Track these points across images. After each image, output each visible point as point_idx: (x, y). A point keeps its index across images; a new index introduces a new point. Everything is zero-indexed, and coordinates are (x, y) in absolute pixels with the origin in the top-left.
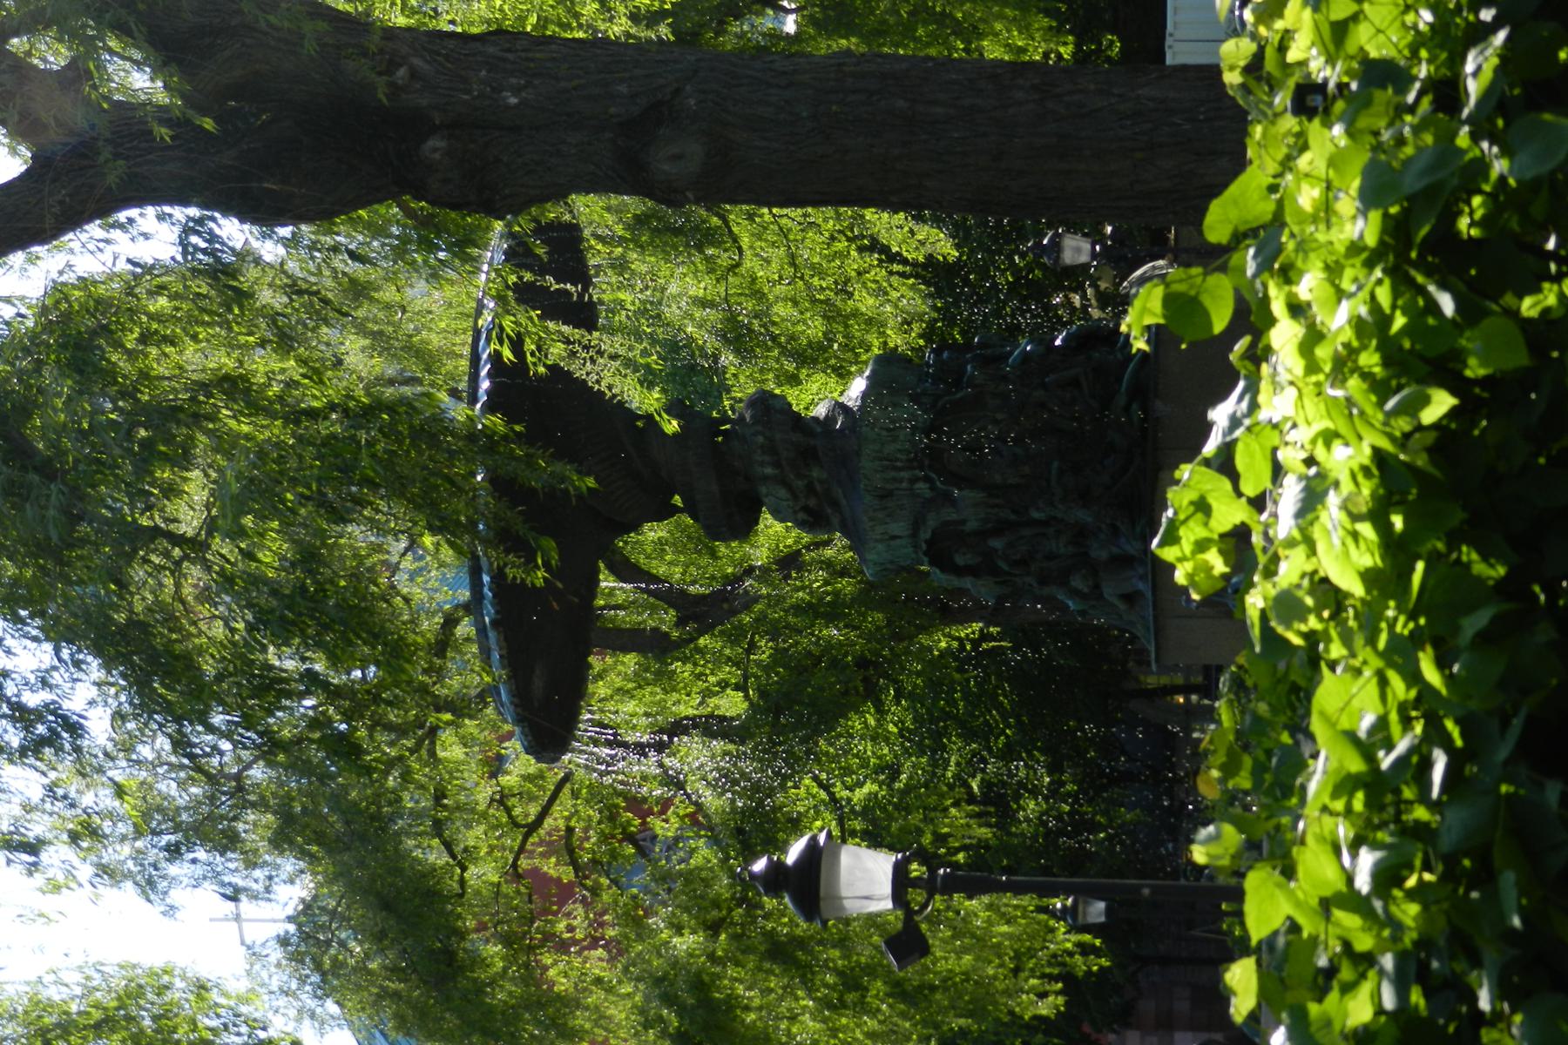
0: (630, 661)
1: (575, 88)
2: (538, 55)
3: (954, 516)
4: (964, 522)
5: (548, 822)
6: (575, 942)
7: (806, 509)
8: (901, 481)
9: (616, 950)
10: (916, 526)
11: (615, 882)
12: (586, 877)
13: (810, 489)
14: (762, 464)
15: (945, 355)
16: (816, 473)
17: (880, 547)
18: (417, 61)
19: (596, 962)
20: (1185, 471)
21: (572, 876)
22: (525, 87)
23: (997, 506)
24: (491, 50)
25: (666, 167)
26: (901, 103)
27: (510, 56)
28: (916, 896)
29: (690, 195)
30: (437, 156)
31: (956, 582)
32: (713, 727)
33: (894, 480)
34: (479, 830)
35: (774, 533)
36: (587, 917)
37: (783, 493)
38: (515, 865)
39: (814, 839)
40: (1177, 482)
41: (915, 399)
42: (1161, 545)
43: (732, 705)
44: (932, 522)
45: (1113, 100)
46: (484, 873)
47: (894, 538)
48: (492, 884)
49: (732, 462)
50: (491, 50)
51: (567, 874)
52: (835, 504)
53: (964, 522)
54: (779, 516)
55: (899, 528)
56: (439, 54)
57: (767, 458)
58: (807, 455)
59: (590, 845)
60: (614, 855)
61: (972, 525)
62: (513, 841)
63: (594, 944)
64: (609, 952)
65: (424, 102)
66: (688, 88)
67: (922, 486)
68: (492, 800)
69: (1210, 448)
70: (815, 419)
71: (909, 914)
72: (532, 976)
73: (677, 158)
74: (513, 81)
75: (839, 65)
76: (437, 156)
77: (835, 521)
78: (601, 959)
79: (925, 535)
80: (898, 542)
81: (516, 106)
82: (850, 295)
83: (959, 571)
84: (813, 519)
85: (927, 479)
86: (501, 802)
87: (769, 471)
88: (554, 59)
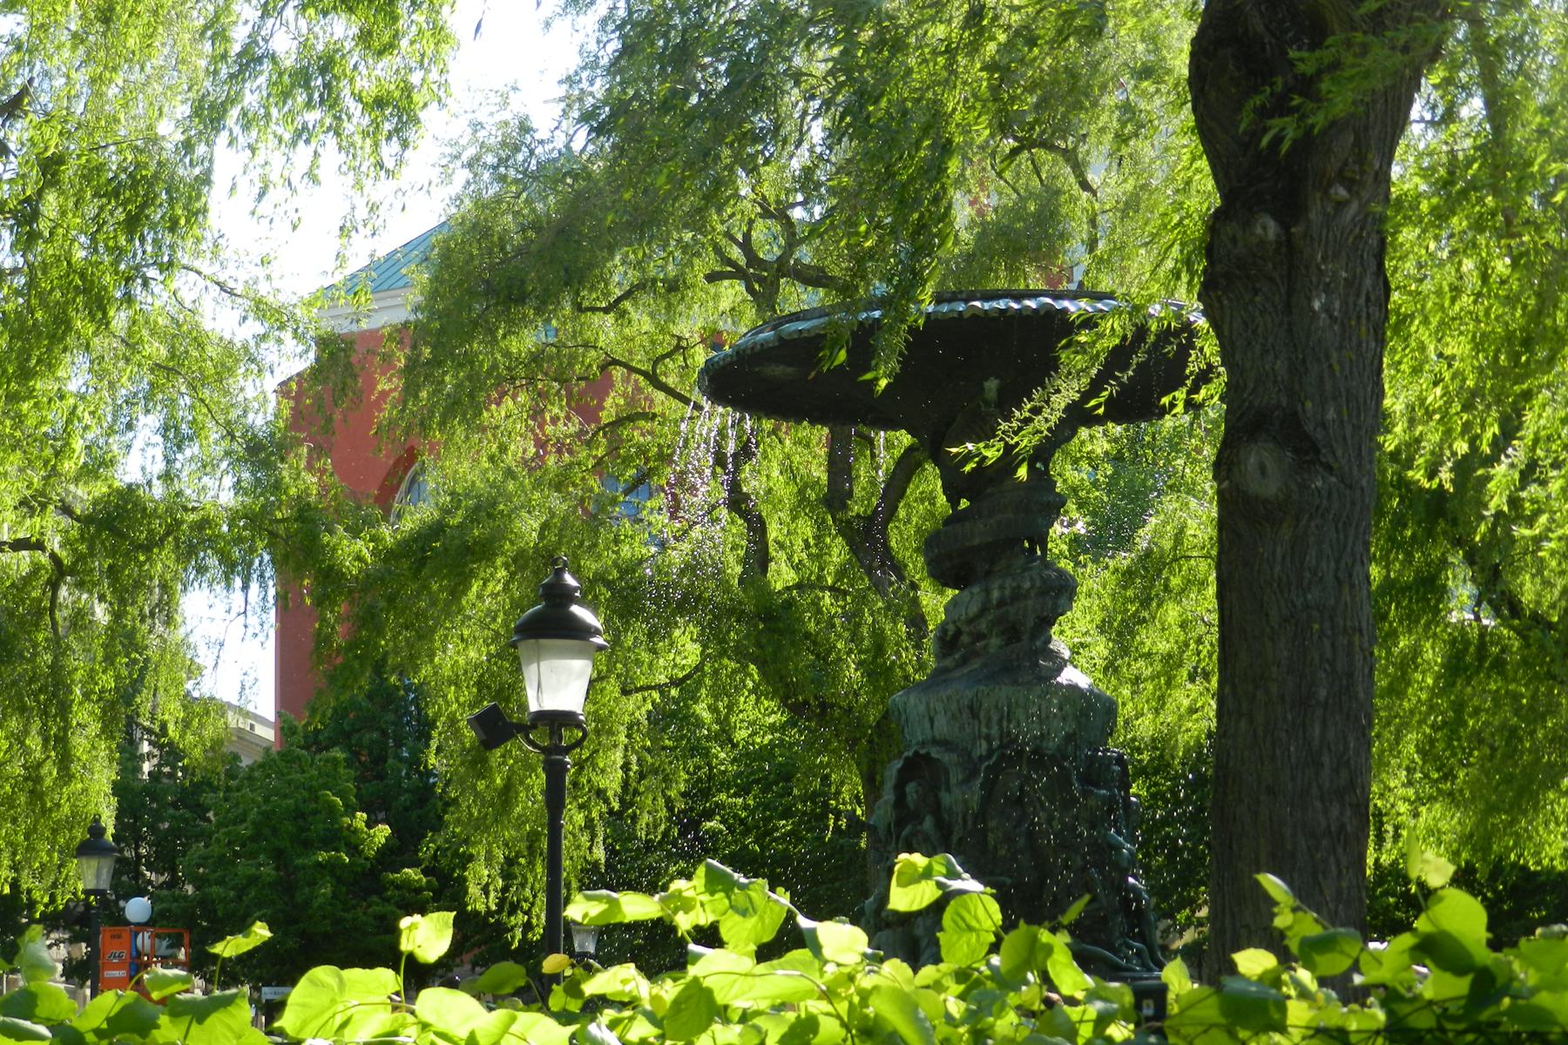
0: (820, 473)
1: (1330, 366)
2: (1363, 329)
3: (953, 780)
4: (948, 790)
5: (660, 396)
6: (541, 427)
7: (958, 633)
8: (988, 727)
9: (533, 465)
10: (945, 744)
11: (600, 462)
12: (605, 435)
13: (980, 636)
14: (1002, 588)
15: (1117, 768)
16: (995, 642)
17: (922, 708)
18: (1354, 206)
19: (521, 448)
20: (783, 898)
21: (605, 421)
22: (1331, 317)
23: (965, 822)
24: (1368, 282)
25: (1252, 460)
26: (1323, 693)
27: (1362, 301)
28: (540, 736)
29: (1226, 484)
30: (1259, 231)
31: (889, 785)
32: (758, 559)
33: (989, 719)
34: (647, 325)
35: (935, 602)
36: (566, 436)
37: (974, 609)
38: (615, 362)
39: (597, 632)
40: (772, 890)
41: (1069, 738)
42: (709, 868)
43: (782, 575)
44: (947, 758)
45: (1331, 906)
46: (605, 330)
47: (932, 721)
48: (596, 340)
49: (999, 552)
50: (1368, 282)
51: (607, 416)
52: (964, 661)
53: (948, 790)
54: (951, 607)
55: (942, 726)
56: (1362, 229)
57: (1007, 592)
58: (1012, 633)
59: (636, 435)
60: (627, 461)
61: (946, 799)
62: (640, 361)
63: (541, 444)
64: (533, 460)
65: (1312, 216)
66: (1333, 479)
67: (983, 747)
68: (680, 339)
69: (804, 922)
70: (1049, 640)
71: (524, 729)
72: (504, 382)
73: (1263, 469)
74: (1337, 305)
75: (1360, 630)
76: (1259, 231)
77: (948, 662)
78: (525, 451)
79: (935, 753)
80: (927, 724)
81: (1312, 309)
82: (1192, 678)
83: (900, 788)
84: (948, 641)
85: (991, 752)
86: (678, 347)
87: (995, 594)
88: (1360, 344)
